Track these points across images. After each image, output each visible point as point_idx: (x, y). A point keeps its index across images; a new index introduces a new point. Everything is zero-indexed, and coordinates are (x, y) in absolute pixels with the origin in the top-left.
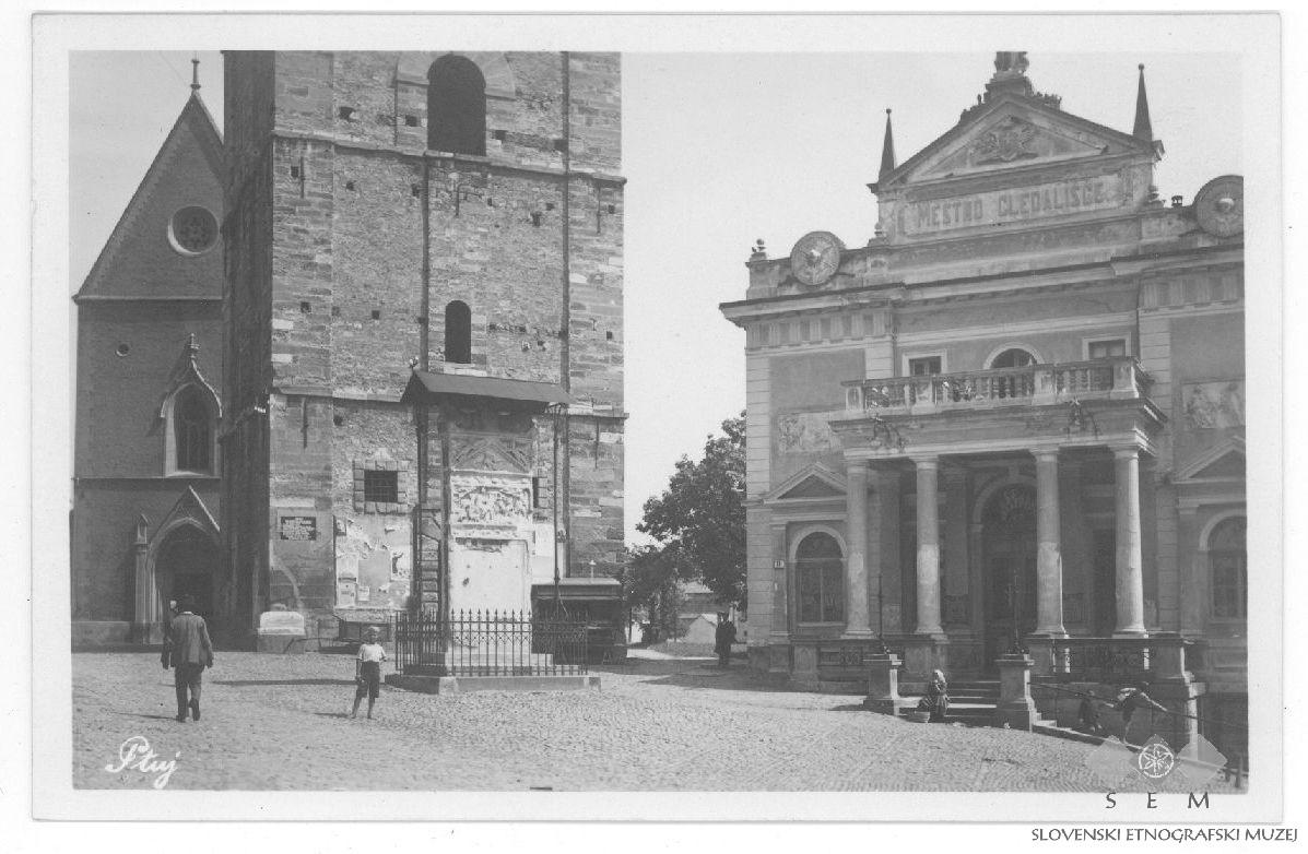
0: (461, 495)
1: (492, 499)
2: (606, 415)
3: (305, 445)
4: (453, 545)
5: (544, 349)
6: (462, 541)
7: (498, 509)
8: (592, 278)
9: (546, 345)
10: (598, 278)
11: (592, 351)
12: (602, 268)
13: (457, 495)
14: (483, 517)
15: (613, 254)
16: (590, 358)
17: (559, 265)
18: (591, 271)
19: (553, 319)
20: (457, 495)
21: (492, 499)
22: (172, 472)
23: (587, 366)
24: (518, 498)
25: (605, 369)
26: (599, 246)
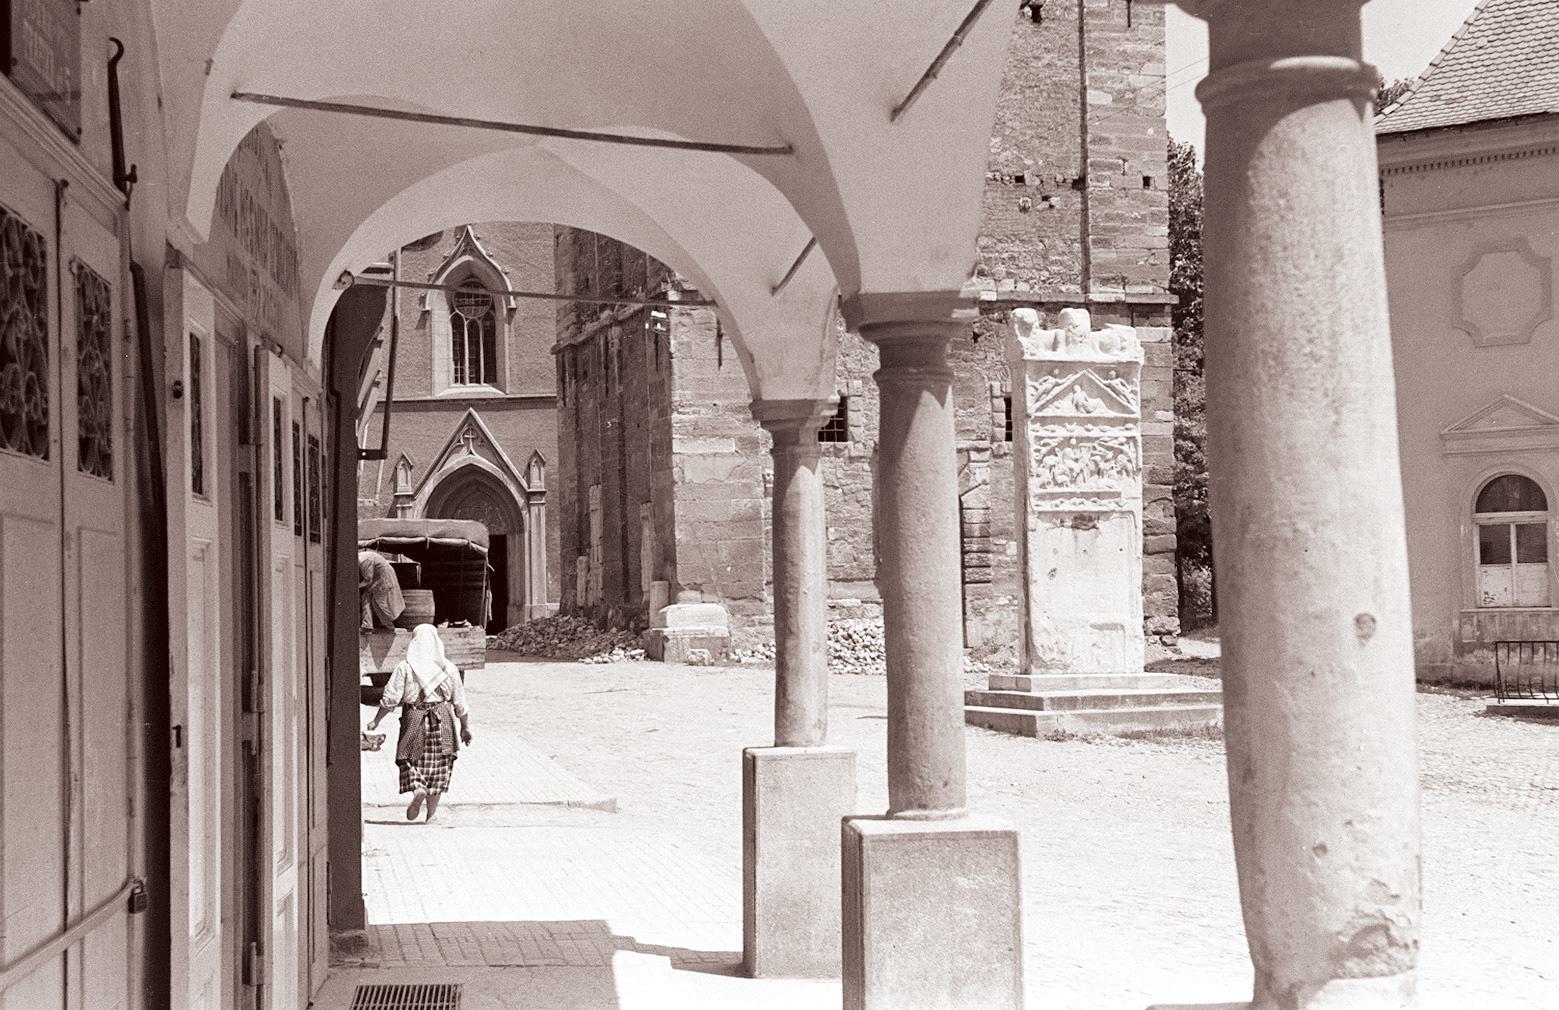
0: (1044, 450)
1: (1085, 454)
2: (1144, 300)
3: (720, 364)
4: (1032, 520)
5: (1051, 207)
6: (1057, 517)
7: (1092, 467)
8: (1119, 97)
9: (1054, 200)
10: (1129, 95)
11: (1121, 206)
12: (1134, 79)
13: (1038, 451)
14: (1074, 481)
15: (1150, 58)
16: (1120, 217)
17: (1070, 77)
18: (1118, 86)
19: (1064, 163)
20: (1038, 451)
21: (1085, 454)
22: (446, 387)
23: (1115, 229)
24: (1122, 452)
25: (1141, 231)
26: (1129, 47)
